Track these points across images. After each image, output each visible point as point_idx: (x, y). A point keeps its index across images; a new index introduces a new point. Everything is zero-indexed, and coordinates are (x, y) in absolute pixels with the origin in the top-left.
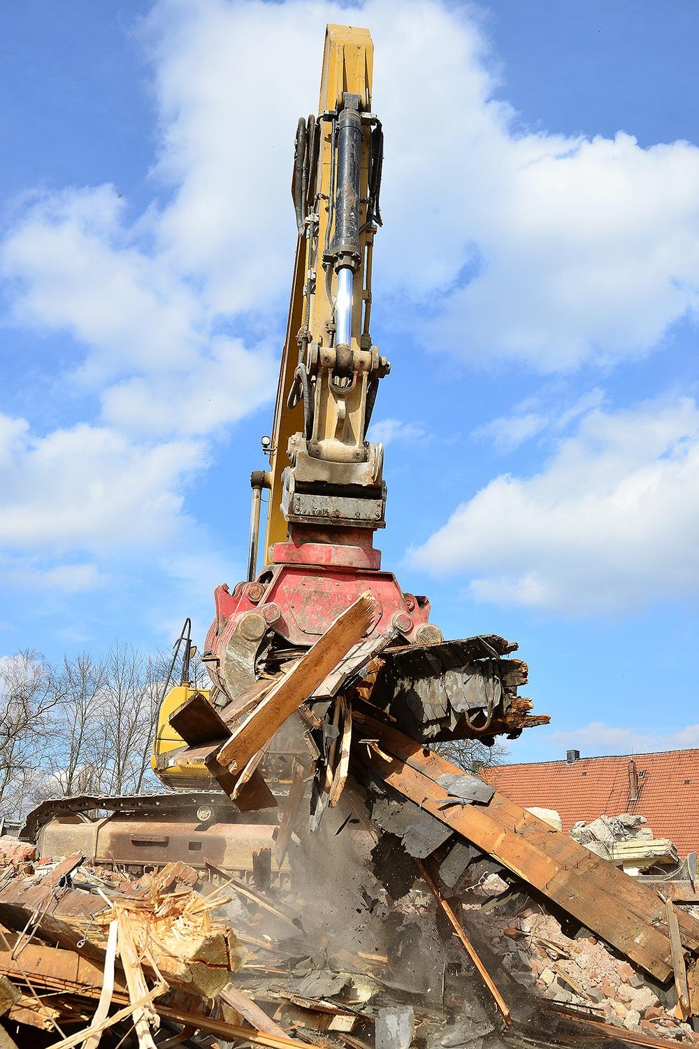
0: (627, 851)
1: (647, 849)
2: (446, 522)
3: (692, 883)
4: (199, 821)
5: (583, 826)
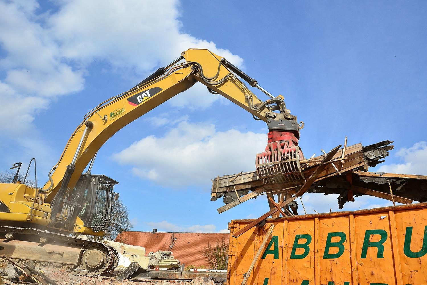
0: (165, 262)
1: (171, 262)
2: (129, 147)
3: (182, 273)
4: (5, 238)
5: (152, 254)
